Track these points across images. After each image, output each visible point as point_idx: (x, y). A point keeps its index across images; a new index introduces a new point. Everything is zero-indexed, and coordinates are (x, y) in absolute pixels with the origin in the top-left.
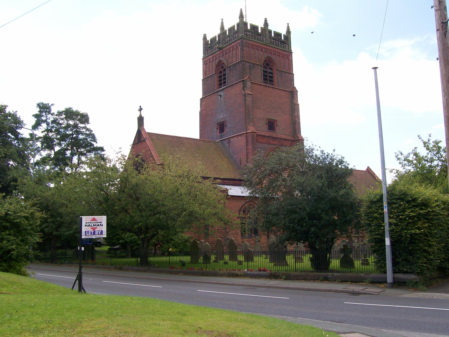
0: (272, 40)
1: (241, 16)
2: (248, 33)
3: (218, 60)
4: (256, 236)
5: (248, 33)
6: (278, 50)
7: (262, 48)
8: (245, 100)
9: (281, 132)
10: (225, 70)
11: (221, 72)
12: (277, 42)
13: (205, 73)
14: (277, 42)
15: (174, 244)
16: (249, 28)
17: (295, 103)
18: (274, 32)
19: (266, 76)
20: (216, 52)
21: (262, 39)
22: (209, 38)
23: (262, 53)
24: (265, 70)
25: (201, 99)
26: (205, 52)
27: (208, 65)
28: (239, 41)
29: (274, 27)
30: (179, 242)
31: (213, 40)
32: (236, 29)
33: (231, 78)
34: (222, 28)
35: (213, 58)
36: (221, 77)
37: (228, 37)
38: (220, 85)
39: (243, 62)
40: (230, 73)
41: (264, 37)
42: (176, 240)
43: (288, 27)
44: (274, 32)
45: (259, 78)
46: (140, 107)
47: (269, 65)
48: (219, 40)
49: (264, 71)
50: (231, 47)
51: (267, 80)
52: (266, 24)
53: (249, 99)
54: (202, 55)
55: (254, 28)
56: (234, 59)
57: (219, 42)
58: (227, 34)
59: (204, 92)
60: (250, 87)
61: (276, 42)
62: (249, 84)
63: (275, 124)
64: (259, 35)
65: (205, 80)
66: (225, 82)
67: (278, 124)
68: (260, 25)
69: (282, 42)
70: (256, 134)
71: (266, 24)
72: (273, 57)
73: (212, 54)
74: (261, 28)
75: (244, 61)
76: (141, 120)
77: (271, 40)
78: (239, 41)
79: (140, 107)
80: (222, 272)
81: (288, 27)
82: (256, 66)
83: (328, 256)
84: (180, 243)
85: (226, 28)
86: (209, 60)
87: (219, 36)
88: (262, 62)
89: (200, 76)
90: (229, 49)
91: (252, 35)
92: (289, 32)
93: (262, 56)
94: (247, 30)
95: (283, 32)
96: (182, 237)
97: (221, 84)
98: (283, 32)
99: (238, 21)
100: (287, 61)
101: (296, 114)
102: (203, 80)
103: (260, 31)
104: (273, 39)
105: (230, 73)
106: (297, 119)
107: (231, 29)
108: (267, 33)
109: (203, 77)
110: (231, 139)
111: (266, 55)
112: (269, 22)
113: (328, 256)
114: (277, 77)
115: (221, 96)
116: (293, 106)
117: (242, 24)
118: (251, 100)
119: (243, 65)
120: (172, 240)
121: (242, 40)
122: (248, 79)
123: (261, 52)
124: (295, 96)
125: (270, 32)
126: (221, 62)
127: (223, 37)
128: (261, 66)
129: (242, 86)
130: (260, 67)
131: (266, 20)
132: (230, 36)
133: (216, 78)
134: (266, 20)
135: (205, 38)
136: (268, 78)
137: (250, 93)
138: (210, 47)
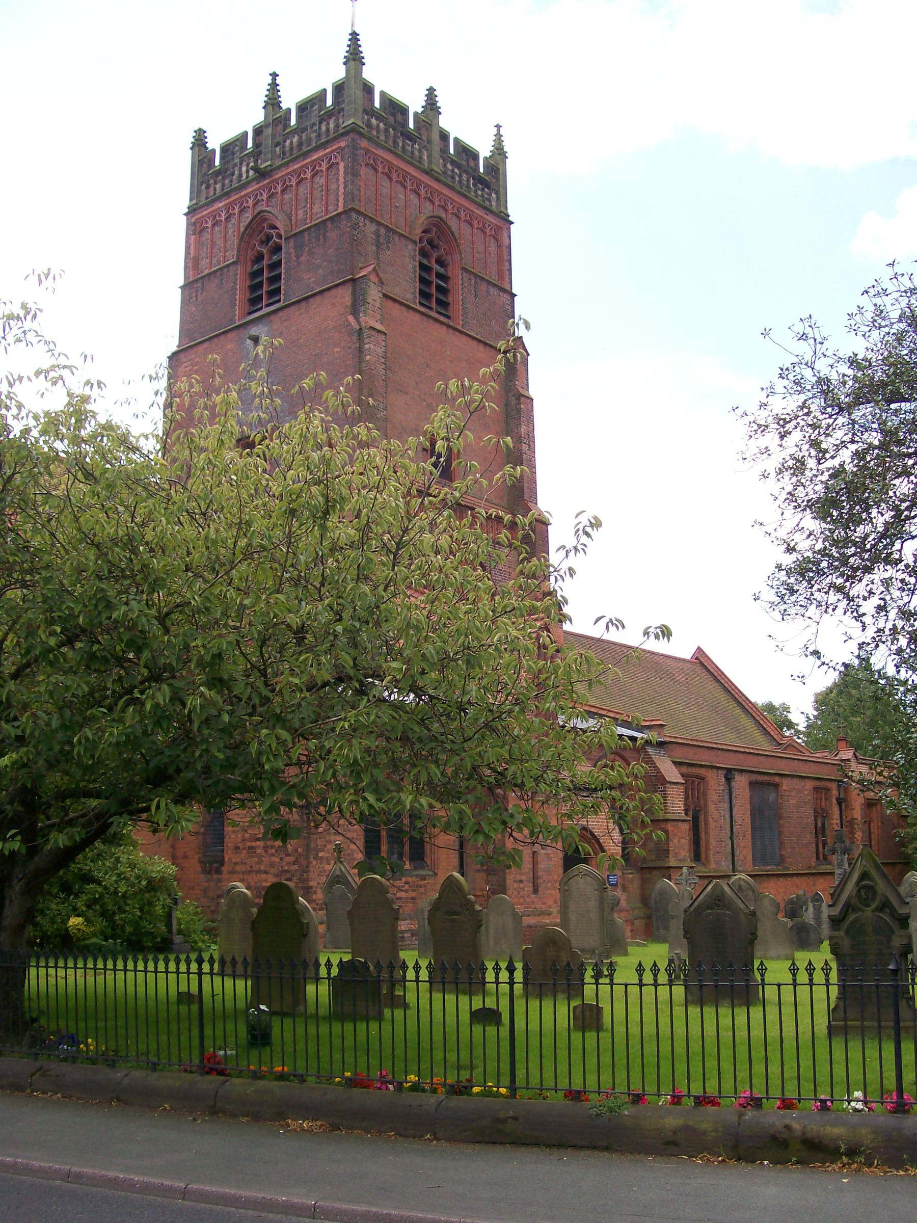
0: (449, 166)
1: (354, 57)
2: (374, 121)
3: (248, 216)
4: (416, 868)
5: (374, 121)
6: (466, 203)
7: (419, 183)
8: (360, 350)
9: (476, 481)
10: (277, 249)
11: (260, 258)
12: (464, 177)
13: (192, 262)
14: (464, 177)
15: (96, 901)
17: (523, 392)
21: (416, 153)
22: (214, 143)
23: (416, 201)
24: (425, 262)
26: (199, 192)
27: (206, 236)
28: (343, 144)
30: (122, 889)
32: (329, 102)
33: (301, 272)
34: (273, 100)
35: (229, 207)
36: (260, 272)
37: (294, 132)
38: (255, 302)
39: (354, 215)
40: (298, 257)
41: (425, 147)
42: (110, 880)
43: (499, 138)
45: (407, 287)
48: (256, 145)
49: (421, 266)
50: (306, 166)
51: (439, 289)
53: (374, 348)
56: (316, 209)
57: (257, 152)
59: (186, 330)
60: (378, 305)
61: (460, 176)
62: (374, 294)
64: (408, 136)
65: (192, 288)
66: (277, 291)
68: (415, 104)
69: (479, 180)
72: (453, 223)
73: (227, 194)
74: (416, 114)
75: (358, 212)
77: (445, 166)
78: (343, 144)
81: (499, 136)
82: (397, 238)
84: (125, 896)
85: (290, 100)
86: (215, 215)
88: (418, 231)
89: (175, 274)
90: (298, 173)
91: (386, 131)
92: (499, 152)
93: (415, 213)
94: (369, 111)
96: (133, 866)
97: (260, 298)
100: (493, 248)
101: (523, 429)
102: (188, 288)
104: (453, 163)
105: (298, 257)
106: (525, 447)
108: (436, 137)
109: (186, 277)
111: (428, 209)
114: (461, 291)
115: (256, 340)
116: (513, 402)
117: (353, 87)
118: (380, 351)
119: (355, 226)
120: (88, 878)
121: (353, 140)
122: (373, 278)
123: (412, 197)
126: (264, 220)
127: (273, 136)
128: (415, 242)
129: (348, 300)
130: (411, 246)
131: (431, 94)
132: (304, 130)
133: (239, 282)
135: (200, 140)
137: (379, 326)
138: (216, 174)
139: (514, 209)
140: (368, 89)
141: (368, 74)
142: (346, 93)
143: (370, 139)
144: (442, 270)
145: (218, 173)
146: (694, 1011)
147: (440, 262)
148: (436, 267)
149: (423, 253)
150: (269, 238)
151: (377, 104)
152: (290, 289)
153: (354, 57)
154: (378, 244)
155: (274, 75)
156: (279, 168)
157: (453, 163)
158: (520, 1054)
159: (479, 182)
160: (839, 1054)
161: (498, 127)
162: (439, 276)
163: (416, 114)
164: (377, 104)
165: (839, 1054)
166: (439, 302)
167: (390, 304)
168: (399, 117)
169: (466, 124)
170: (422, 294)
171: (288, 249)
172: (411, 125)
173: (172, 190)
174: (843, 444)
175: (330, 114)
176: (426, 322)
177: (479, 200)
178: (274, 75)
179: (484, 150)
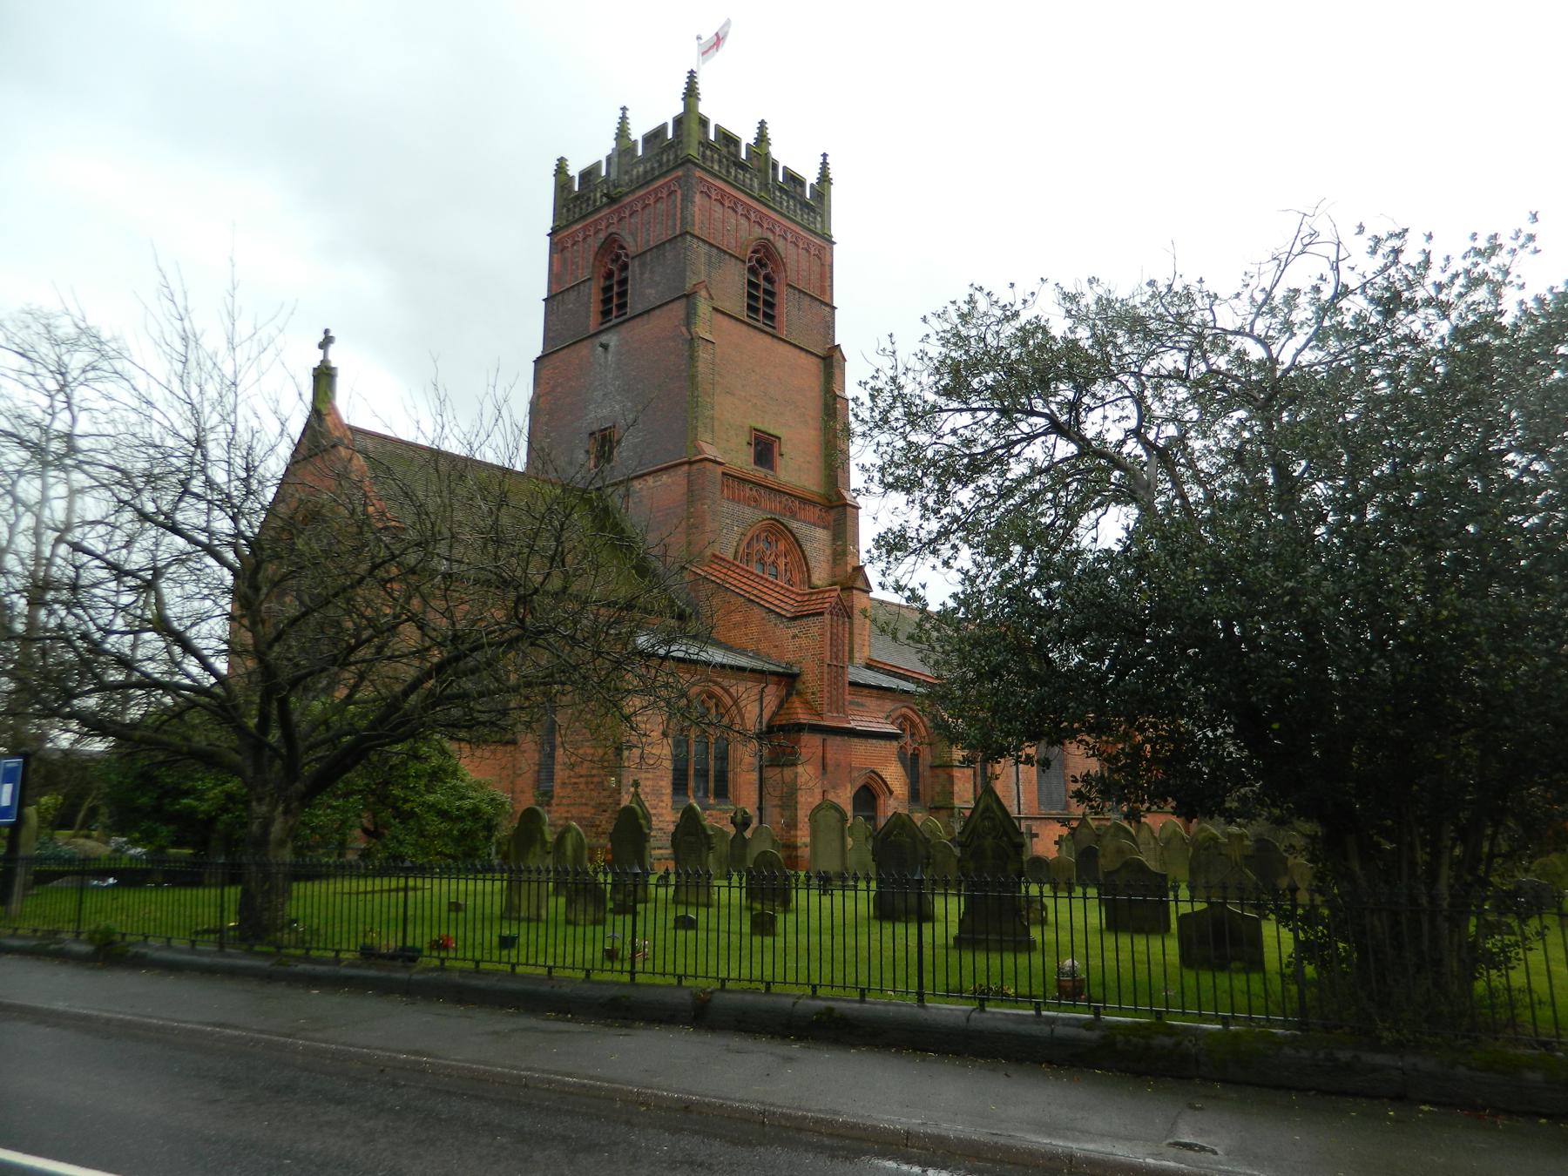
1: (691, 93)
3: (602, 236)
6: (793, 226)
10: (625, 267)
11: (610, 275)
19: (756, 298)
20: (598, 210)
22: (574, 170)
25: (538, 361)
28: (680, 173)
31: (588, 175)
32: (670, 135)
34: (622, 132)
35: (585, 228)
38: (606, 314)
40: (642, 274)
46: (326, 331)
47: (765, 266)
49: (750, 283)
51: (766, 303)
58: (640, 153)
62: (703, 308)
63: (776, 450)
64: (741, 166)
66: (622, 306)
67: (784, 450)
68: (747, 136)
69: (806, 205)
70: (720, 469)
71: (762, 138)
72: (780, 244)
73: (583, 217)
74: (748, 145)
75: (693, 236)
76: (324, 377)
78: (680, 173)
79: (326, 331)
85: (637, 133)
87: (609, 158)
92: (825, 178)
94: (705, 144)
99: (679, 108)
104: (781, 189)
109: (549, 290)
110: (636, 483)
111: (757, 231)
114: (788, 307)
115: (605, 347)
117: (690, 119)
123: (743, 221)
124: (837, 371)
134: (762, 124)
136: (762, 306)
139: (837, 231)
140: (704, 122)
141: (704, 108)
142: (685, 127)
143: (704, 169)
144: (769, 287)
145: (577, 197)
146: (1110, 940)
147: (768, 278)
148: (763, 283)
149: (752, 270)
150: (618, 257)
151: (712, 137)
152: (635, 304)
153: (691, 93)
154: (710, 264)
155: (624, 109)
156: (627, 194)
157: (781, 189)
158: (927, 951)
159: (807, 203)
160: (875, 937)
161: (825, 155)
162: (766, 292)
163: (748, 145)
164: (712, 137)
165: (875, 937)
166: (766, 315)
167: (720, 316)
168: (732, 149)
169: (794, 154)
170: (750, 307)
171: (634, 266)
172: (743, 156)
173: (538, 212)
174: (397, 754)
175: (671, 145)
176: (752, 332)
177: (805, 223)
178: (624, 109)
179: (811, 176)
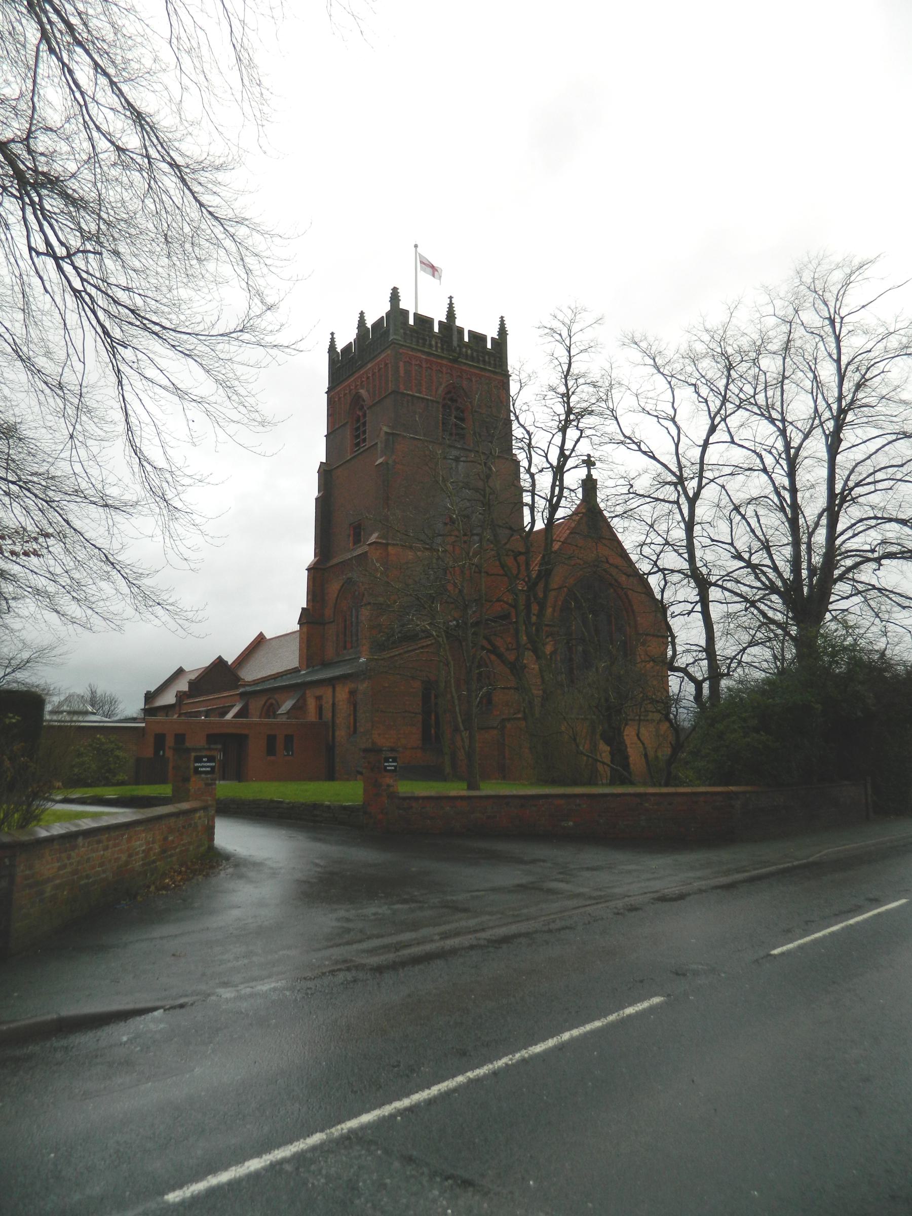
16: (466, 339)
18: (470, 331)
22: (340, 347)
29: (466, 322)
36: (357, 429)
44: (470, 331)
52: (451, 314)
54: (327, 386)
55: (424, 322)
68: (439, 315)
71: (451, 314)
80: (27, 290)
83: (433, 731)
92: (503, 331)
95: (491, 332)
98: (491, 332)
99: (387, 307)
103: (489, 346)
107: (378, 324)
112: (508, 327)
113: (433, 731)
117: (396, 313)
125: (460, 331)
135: (332, 348)
138: (342, 365)
